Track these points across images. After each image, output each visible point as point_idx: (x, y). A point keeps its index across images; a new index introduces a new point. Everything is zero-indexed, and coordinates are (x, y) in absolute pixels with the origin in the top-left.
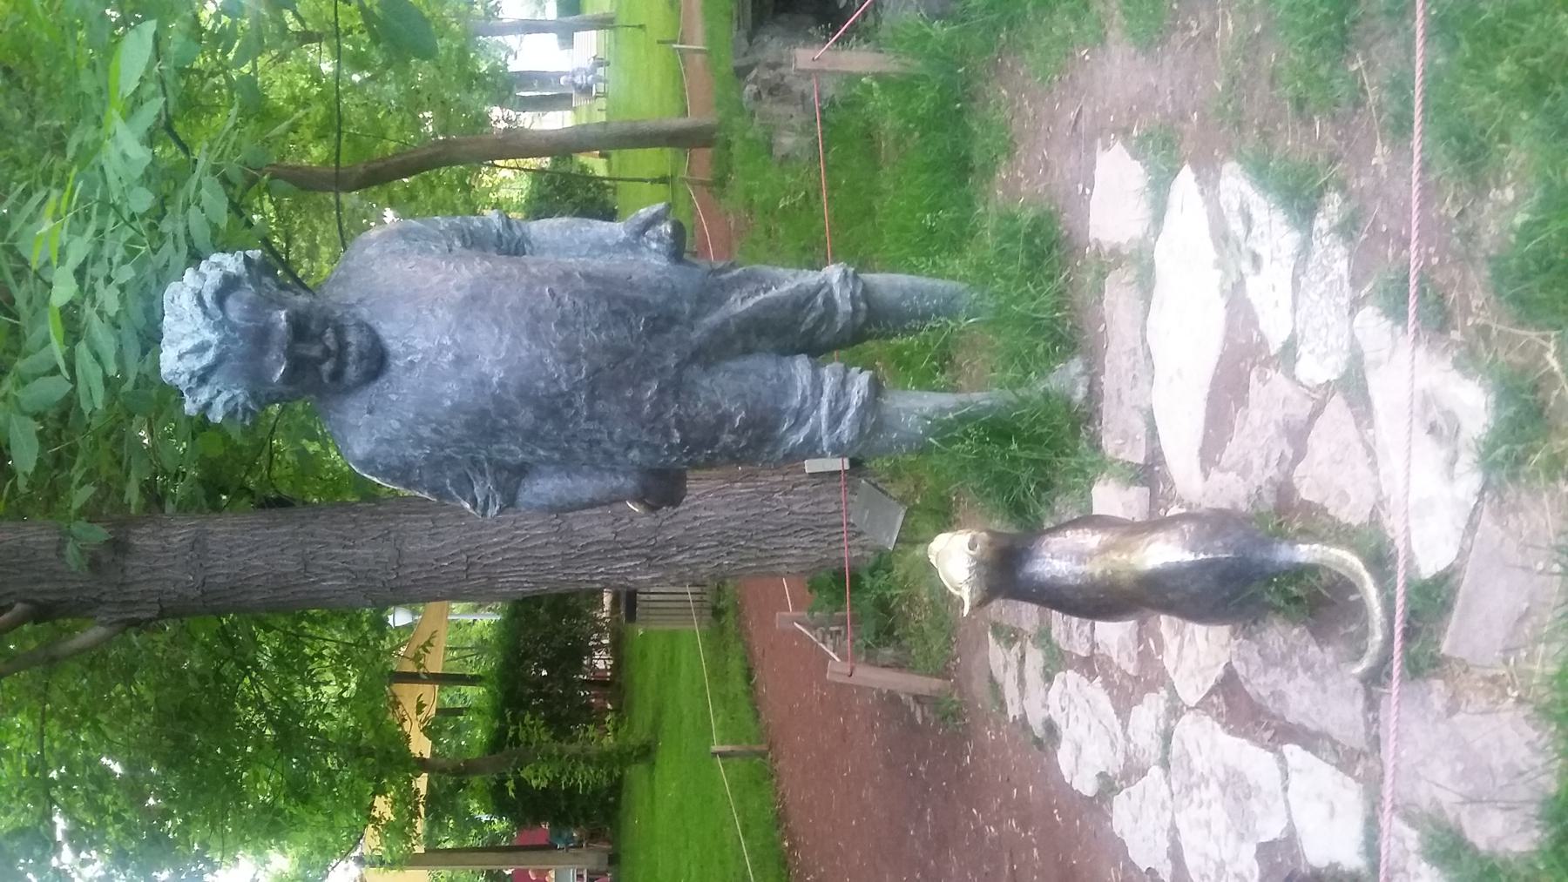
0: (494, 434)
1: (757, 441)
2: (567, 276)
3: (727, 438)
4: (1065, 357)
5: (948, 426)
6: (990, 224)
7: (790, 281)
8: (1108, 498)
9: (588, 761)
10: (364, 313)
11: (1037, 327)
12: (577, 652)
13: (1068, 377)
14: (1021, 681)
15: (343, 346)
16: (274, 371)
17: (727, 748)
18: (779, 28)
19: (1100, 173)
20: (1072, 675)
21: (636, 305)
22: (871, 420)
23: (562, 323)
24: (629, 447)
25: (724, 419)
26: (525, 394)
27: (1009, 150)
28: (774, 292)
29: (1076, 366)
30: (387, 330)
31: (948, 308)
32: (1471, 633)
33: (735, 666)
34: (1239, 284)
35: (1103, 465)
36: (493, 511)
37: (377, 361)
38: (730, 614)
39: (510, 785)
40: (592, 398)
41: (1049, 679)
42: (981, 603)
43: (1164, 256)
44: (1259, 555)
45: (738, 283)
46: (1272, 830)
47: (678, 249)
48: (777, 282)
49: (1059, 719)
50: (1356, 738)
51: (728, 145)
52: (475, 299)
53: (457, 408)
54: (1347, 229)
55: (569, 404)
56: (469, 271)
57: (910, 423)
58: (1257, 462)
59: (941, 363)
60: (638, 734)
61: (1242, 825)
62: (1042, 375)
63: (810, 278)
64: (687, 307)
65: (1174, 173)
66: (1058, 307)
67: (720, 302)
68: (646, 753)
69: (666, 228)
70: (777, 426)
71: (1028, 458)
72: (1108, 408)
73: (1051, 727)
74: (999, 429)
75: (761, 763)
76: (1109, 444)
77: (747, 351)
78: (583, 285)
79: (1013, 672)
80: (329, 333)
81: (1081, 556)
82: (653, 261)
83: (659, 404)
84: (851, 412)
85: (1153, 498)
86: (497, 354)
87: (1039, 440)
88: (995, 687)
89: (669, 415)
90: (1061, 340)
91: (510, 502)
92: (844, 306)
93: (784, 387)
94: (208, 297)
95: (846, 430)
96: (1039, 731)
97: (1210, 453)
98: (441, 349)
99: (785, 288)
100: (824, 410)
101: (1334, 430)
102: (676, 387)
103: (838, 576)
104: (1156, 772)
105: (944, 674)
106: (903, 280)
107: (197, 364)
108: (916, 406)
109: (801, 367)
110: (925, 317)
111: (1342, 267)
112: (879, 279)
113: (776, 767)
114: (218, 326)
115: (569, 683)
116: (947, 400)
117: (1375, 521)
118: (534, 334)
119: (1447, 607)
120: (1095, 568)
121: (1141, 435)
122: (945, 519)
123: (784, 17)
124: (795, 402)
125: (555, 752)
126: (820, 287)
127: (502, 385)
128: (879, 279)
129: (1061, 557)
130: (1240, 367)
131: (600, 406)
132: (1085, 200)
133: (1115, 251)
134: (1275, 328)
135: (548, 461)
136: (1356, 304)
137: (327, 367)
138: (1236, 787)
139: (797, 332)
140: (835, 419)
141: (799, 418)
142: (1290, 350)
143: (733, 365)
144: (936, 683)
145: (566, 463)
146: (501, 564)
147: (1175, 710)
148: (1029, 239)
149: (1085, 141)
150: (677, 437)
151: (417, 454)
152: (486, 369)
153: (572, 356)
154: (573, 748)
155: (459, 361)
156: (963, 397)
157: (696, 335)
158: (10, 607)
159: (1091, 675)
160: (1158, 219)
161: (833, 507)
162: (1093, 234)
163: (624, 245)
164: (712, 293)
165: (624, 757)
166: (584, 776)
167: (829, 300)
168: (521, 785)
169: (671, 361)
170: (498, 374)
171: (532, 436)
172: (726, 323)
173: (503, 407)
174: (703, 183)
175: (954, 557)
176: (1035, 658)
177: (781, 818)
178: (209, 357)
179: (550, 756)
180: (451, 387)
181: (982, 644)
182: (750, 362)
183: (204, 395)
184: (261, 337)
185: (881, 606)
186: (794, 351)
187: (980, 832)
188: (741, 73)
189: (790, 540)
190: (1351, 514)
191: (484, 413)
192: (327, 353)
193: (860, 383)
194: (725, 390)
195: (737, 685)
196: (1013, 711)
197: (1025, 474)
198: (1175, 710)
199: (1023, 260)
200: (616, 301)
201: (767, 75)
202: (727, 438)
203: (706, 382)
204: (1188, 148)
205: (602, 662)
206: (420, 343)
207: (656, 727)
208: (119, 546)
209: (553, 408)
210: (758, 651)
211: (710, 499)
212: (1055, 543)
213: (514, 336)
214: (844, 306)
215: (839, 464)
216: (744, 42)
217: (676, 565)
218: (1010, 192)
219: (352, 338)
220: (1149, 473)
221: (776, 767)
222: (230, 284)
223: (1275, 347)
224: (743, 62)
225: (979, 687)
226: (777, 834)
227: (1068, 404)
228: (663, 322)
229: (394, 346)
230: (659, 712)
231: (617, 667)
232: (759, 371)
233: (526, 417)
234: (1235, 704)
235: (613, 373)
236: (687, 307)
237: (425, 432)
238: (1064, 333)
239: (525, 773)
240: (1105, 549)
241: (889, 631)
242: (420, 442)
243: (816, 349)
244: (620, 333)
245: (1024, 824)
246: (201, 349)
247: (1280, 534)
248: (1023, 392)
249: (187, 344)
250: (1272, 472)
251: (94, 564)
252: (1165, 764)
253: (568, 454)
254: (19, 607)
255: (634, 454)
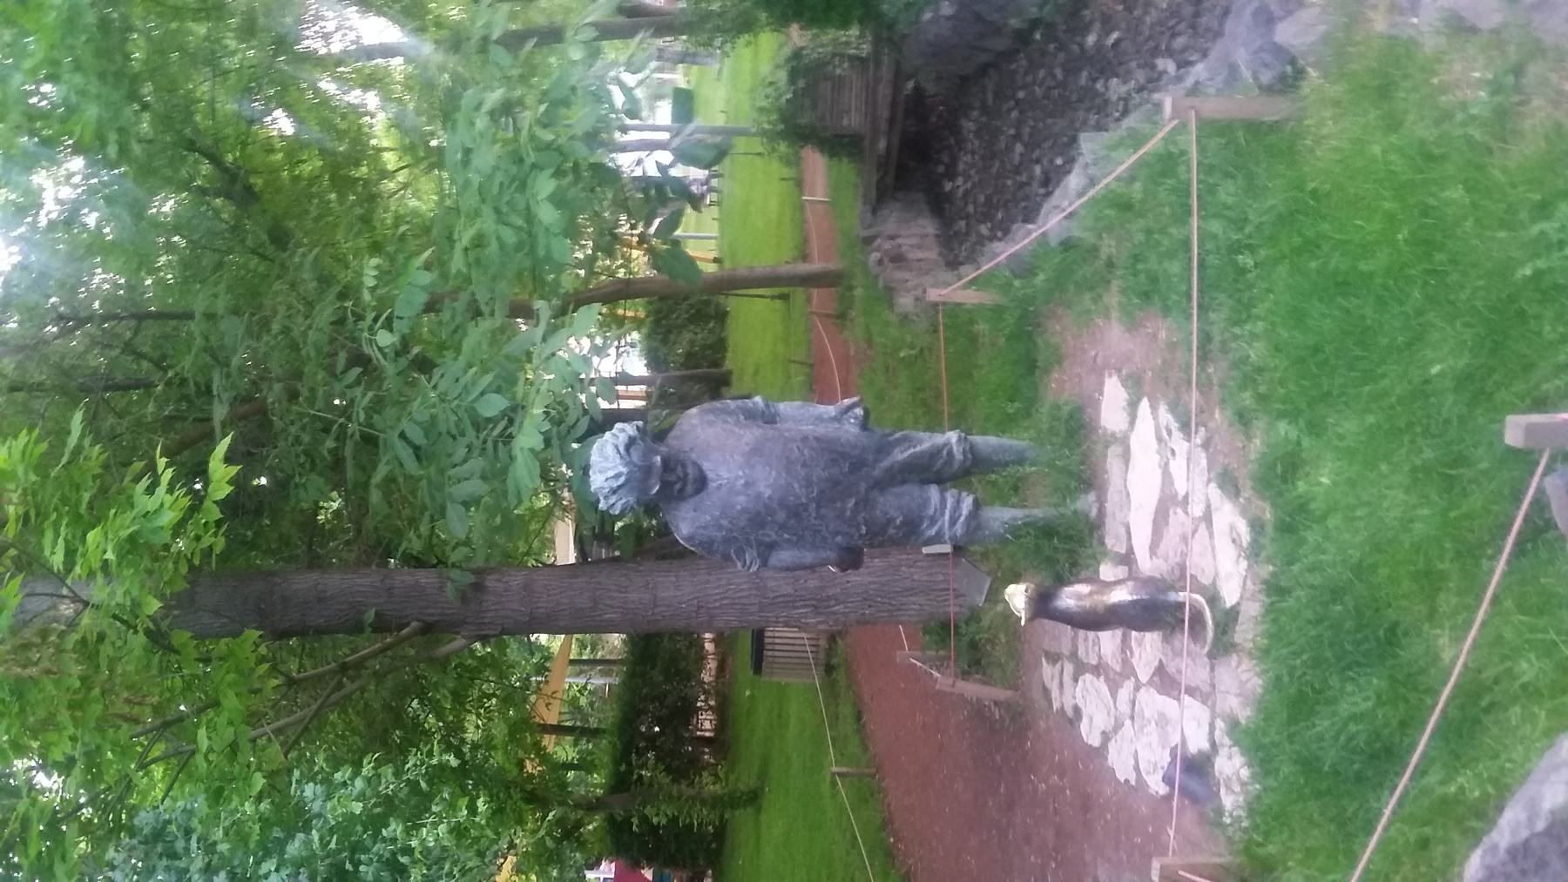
0: (762, 525)
1: (910, 531)
2: (805, 439)
3: (891, 531)
4: (1086, 492)
5: (1019, 528)
6: (1045, 410)
7: (928, 441)
8: (1107, 571)
9: (703, 802)
10: (694, 456)
11: (1070, 474)
12: (687, 711)
13: (1087, 503)
14: (1061, 683)
15: (686, 475)
16: (651, 488)
17: (844, 770)
18: (898, 205)
19: (1106, 389)
20: (1088, 677)
21: (844, 455)
22: (973, 523)
23: (804, 465)
24: (837, 533)
25: (890, 521)
26: (783, 504)
27: (1060, 362)
28: (918, 449)
29: (1092, 497)
30: (706, 466)
31: (1020, 460)
32: (1245, 633)
33: (846, 710)
34: (1167, 464)
35: (1105, 554)
36: (754, 569)
37: (702, 482)
38: (842, 670)
39: (635, 821)
40: (819, 507)
41: (1076, 680)
42: (1030, 620)
43: (1134, 442)
44: (1162, 597)
45: (899, 442)
46: (1175, 739)
47: (865, 424)
48: (920, 442)
49: (1081, 705)
50: (1206, 688)
51: (851, 288)
52: (756, 450)
53: (744, 510)
54: (1206, 445)
55: (806, 510)
56: (751, 434)
57: (996, 526)
58: (1171, 554)
59: (1015, 491)
60: (745, 779)
61: (1164, 737)
62: (1073, 501)
63: (939, 439)
64: (871, 457)
65: (1140, 400)
66: (1082, 463)
67: (889, 454)
68: (754, 798)
69: (859, 411)
70: (920, 525)
71: (1065, 546)
72: (1109, 521)
73: (1077, 710)
74: (1047, 531)
75: (868, 785)
76: (1109, 542)
77: (904, 482)
78: (815, 444)
79: (1056, 681)
80: (679, 469)
81: (1079, 597)
82: (850, 429)
83: (855, 511)
84: (962, 519)
85: (1130, 570)
86: (767, 482)
87: (1070, 538)
88: (1046, 692)
89: (860, 518)
90: (1084, 482)
91: (764, 563)
92: (959, 456)
93: (925, 503)
94: (622, 449)
95: (959, 529)
96: (1070, 712)
97: (1153, 549)
98: (737, 478)
99: (926, 446)
100: (947, 517)
101: (1199, 542)
102: (865, 503)
103: (945, 626)
104: (1128, 722)
105: (1015, 688)
106: (992, 440)
107: (615, 484)
108: (1000, 516)
109: (933, 492)
110: (1007, 464)
111: (1204, 462)
112: (978, 439)
113: (883, 784)
114: (626, 465)
115: (680, 740)
116: (1019, 513)
117: (1214, 583)
118: (788, 471)
119: (1236, 620)
120: (1087, 603)
121: (1124, 538)
122: (1016, 579)
123: (900, 195)
124: (931, 512)
125: (675, 793)
126: (945, 445)
127: (770, 498)
128: (978, 439)
129: (1071, 597)
130: (1168, 503)
131: (823, 511)
132: (1097, 403)
133: (1113, 434)
134: (1181, 487)
135: (789, 541)
136: (1209, 481)
137: (678, 486)
138: (1162, 721)
139: (930, 470)
140: (953, 522)
141: (933, 521)
142: (1185, 501)
143: (896, 490)
144: (1009, 693)
145: (798, 543)
146: (719, 608)
147: (1137, 688)
148: (1067, 422)
149: (1099, 373)
150: (864, 530)
151: (718, 535)
152: (762, 489)
153: (808, 483)
154: (691, 792)
155: (747, 485)
156: (1026, 512)
157: (877, 473)
158: (408, 624)
159: (1098, 676)
160: (1132, 422)
161: (941, 578)
162: (1103, 423)
163: (836, 419)
164: (884, 449)
165: (733, 801)
166: (701, 816)
167: (950, 453)
168: (645, 820)
169: (863, 486)
170: (768, 493)
171: (783, 527)
172: (892, 467)
173: (770, 512)
174: (828, 316)
175: (1017, 596)
176: (1069, 668)
177: (887, 823)
178: (622, 479)
179: (671, 797)
180: (742, 499)
181: (1038, 665)
182: (907, 488)
183: (613, 500)
184: (647, 470)
185: (972, 643)
186: (926, 482)
187: (1035, 790)
188: (868, 241)
189: (913, 599)
190: (1206, 580)
191: (759, 513)
192: (679, 479)
193: (967, 502)
194: (891, 504)
195: (848, 726)
196: (1056, 705)
197: (1062, 557)
198: (1137, 688)
199: (1063, 433)
200: (831, 451)
201: (887, 245)
202: (891, 531)
203: (881, 500)
204: (1147, 388)
205: (706, 724)
206: (725, 475)
207: (763, 775)
208: (478, 587)
209: (796, 512)
210: (867, 698)
211: (874, 570)
212: (1068, 590)
213: (778, 473)
214: (959, 456)
215: (946, 548)
216: (869, 215)
217: (835, 613)
218: (1058, 388)
219: (690, 470)
220: (1127, 559)
221: (883, 784)
222: (631, 442)
223: (1180, 498)
224: (866, 233)
225: (1037, 695)
226: (884, 834)
227: (1087, 516)
228: (858, 465)
229: (710, 475)
230: (766, 762)
231: (722, 725)
232: (910, 492)
233: (781, 516)
234: (1165, 681)
235: (831, 492)
236: (871, 457)
237: (725, 522)
238: (1087, 478)
239: (648, 811)
240: (1091, 594)
241: (978, 663)
242: (720, 528)
243: (940, 480)
244: (835, 471)
245: (1061, 777)
246: (617, 476)
247: (1172, 588)
248: (1062, 510)
249: (611, 473)
250: (1178, 559)
251: (464, 598)
252: (1132, 718)
253: (801, 538)
254: (414, 624)
255: (839, 539)
